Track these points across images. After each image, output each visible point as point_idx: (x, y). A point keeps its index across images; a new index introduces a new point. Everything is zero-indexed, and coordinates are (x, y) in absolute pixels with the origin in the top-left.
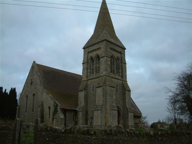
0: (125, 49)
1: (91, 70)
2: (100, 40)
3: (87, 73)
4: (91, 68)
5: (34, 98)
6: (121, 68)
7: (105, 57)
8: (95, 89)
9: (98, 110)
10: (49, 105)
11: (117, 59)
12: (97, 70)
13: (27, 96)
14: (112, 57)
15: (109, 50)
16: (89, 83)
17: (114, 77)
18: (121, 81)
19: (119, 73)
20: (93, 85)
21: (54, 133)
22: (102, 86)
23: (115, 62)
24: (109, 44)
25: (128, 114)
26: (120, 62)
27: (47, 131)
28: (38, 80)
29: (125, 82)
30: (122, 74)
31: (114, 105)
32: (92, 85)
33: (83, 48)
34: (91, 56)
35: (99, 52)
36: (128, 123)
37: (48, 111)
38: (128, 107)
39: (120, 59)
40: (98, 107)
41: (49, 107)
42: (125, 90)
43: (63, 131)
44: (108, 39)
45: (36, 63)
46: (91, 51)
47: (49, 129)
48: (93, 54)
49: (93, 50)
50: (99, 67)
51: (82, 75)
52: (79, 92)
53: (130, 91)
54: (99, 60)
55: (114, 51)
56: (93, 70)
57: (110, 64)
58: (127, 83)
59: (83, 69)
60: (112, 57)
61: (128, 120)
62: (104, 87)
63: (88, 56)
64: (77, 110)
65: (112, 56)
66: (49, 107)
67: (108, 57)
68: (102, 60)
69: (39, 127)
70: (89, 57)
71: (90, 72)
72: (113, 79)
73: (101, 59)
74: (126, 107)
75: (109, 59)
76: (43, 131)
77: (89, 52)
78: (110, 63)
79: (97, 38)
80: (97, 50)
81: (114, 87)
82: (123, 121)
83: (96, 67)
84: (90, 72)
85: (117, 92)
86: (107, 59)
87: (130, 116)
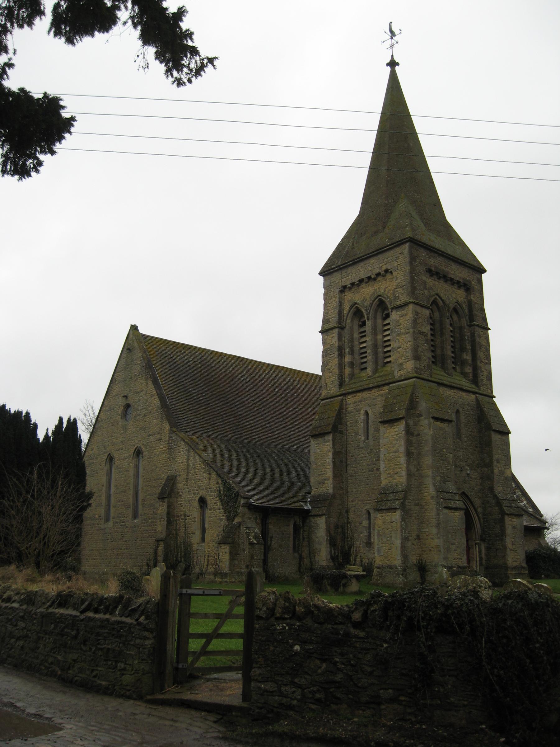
0: (484, 271)
1: (357, 357)
2: (387, 242)
3: (341, 366)
4: (356, 349)
5: (137, 467)
6: (469, 347)
7: (411, 307)
8: (377, 430)
9: (389, 510)
10: (201, 493)
11: (455, 310)
12: (381, 355)
13: (111, 459)
14: (435, 304)
15: (425, 278)
16: (351, 408)
17: (446, 379)
18: (473, 397)
19: (463, 363)
20: (367, 413)
21: (320, 623)
22: (402, 418)
23: (448, 321)
24: (423, 253)
25: (502, 522)
26: (465, 322)
27: (294, 615)
28: (147, 397)
29: (487, 399)
30: (475, 369)
31: (451, 487)
32: (362, 412)
33: (322, 273)
34: (355, 303)
35: (384, 287)
36: (504, 557)
37: (195, 513)
38: (500, 496)
39: (466, 311)
40: (391, 496)
41: (202, 502)
42: (488, 432)
43: (357, 616)
44: (419, 237)
45: (142, 330)
46: (353, 284)
47: (300, 609)
48: (367, 293)
49: (361, 281)
50: (387, 343)
51: (320, 374)
52: (313, 442)
53: (509, 432)
54: (388, 316)
55: (435, 277)
56: (363, 354)
57: (429, 333)
58: (495, 404)
59: (325, 354)
60: (437, 305)
61: (505, 548)
62: (411, 422)
63: (341, 304)
64: (308, 511)
65: (435, 302)
66: (202, 502)
67: (422, 306)
68: (402, 320)
69: (259, 605)
70: (347, 308)
71: (352, 364)
72: (442, 389)
73: (395, 315)
74: (495, 497)
75: (427, 312)
76: (277, 619)
77: (345, 287)
78: (429, 327)
79: (376, 233)
80: (375, 279)
81: (450, 421)
82: (483, 551)
83: (375, 346)
84: (352, 364)
85: (459, 438)
86: (417, 313)
87: (509, 530)
